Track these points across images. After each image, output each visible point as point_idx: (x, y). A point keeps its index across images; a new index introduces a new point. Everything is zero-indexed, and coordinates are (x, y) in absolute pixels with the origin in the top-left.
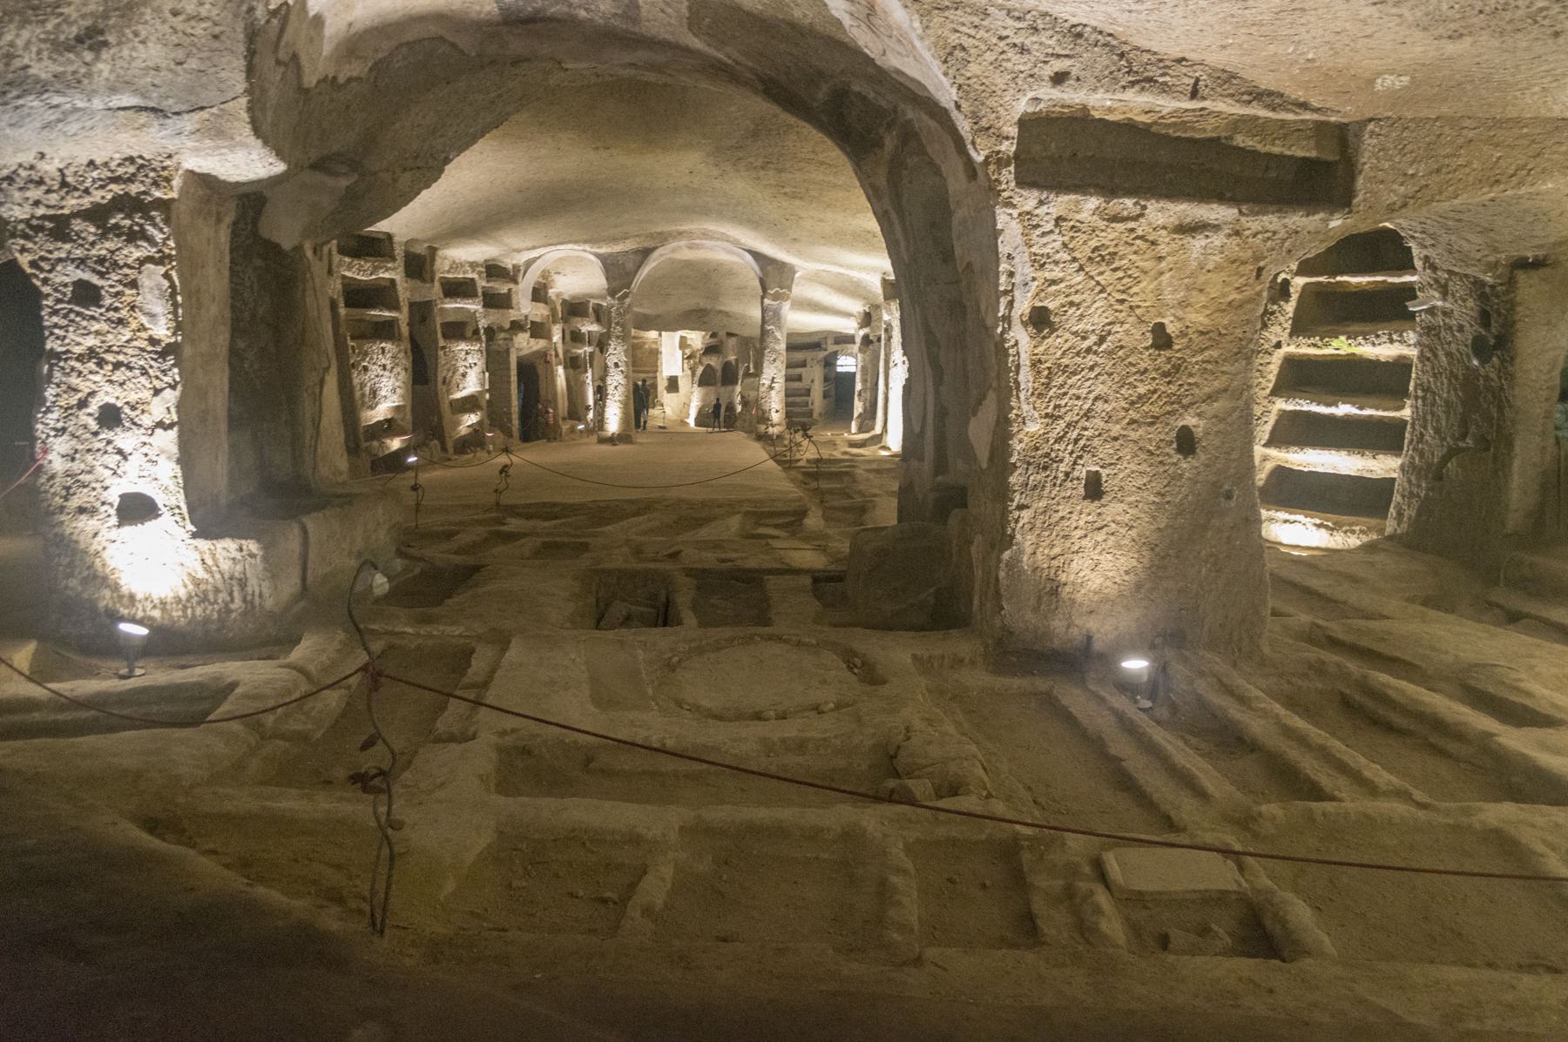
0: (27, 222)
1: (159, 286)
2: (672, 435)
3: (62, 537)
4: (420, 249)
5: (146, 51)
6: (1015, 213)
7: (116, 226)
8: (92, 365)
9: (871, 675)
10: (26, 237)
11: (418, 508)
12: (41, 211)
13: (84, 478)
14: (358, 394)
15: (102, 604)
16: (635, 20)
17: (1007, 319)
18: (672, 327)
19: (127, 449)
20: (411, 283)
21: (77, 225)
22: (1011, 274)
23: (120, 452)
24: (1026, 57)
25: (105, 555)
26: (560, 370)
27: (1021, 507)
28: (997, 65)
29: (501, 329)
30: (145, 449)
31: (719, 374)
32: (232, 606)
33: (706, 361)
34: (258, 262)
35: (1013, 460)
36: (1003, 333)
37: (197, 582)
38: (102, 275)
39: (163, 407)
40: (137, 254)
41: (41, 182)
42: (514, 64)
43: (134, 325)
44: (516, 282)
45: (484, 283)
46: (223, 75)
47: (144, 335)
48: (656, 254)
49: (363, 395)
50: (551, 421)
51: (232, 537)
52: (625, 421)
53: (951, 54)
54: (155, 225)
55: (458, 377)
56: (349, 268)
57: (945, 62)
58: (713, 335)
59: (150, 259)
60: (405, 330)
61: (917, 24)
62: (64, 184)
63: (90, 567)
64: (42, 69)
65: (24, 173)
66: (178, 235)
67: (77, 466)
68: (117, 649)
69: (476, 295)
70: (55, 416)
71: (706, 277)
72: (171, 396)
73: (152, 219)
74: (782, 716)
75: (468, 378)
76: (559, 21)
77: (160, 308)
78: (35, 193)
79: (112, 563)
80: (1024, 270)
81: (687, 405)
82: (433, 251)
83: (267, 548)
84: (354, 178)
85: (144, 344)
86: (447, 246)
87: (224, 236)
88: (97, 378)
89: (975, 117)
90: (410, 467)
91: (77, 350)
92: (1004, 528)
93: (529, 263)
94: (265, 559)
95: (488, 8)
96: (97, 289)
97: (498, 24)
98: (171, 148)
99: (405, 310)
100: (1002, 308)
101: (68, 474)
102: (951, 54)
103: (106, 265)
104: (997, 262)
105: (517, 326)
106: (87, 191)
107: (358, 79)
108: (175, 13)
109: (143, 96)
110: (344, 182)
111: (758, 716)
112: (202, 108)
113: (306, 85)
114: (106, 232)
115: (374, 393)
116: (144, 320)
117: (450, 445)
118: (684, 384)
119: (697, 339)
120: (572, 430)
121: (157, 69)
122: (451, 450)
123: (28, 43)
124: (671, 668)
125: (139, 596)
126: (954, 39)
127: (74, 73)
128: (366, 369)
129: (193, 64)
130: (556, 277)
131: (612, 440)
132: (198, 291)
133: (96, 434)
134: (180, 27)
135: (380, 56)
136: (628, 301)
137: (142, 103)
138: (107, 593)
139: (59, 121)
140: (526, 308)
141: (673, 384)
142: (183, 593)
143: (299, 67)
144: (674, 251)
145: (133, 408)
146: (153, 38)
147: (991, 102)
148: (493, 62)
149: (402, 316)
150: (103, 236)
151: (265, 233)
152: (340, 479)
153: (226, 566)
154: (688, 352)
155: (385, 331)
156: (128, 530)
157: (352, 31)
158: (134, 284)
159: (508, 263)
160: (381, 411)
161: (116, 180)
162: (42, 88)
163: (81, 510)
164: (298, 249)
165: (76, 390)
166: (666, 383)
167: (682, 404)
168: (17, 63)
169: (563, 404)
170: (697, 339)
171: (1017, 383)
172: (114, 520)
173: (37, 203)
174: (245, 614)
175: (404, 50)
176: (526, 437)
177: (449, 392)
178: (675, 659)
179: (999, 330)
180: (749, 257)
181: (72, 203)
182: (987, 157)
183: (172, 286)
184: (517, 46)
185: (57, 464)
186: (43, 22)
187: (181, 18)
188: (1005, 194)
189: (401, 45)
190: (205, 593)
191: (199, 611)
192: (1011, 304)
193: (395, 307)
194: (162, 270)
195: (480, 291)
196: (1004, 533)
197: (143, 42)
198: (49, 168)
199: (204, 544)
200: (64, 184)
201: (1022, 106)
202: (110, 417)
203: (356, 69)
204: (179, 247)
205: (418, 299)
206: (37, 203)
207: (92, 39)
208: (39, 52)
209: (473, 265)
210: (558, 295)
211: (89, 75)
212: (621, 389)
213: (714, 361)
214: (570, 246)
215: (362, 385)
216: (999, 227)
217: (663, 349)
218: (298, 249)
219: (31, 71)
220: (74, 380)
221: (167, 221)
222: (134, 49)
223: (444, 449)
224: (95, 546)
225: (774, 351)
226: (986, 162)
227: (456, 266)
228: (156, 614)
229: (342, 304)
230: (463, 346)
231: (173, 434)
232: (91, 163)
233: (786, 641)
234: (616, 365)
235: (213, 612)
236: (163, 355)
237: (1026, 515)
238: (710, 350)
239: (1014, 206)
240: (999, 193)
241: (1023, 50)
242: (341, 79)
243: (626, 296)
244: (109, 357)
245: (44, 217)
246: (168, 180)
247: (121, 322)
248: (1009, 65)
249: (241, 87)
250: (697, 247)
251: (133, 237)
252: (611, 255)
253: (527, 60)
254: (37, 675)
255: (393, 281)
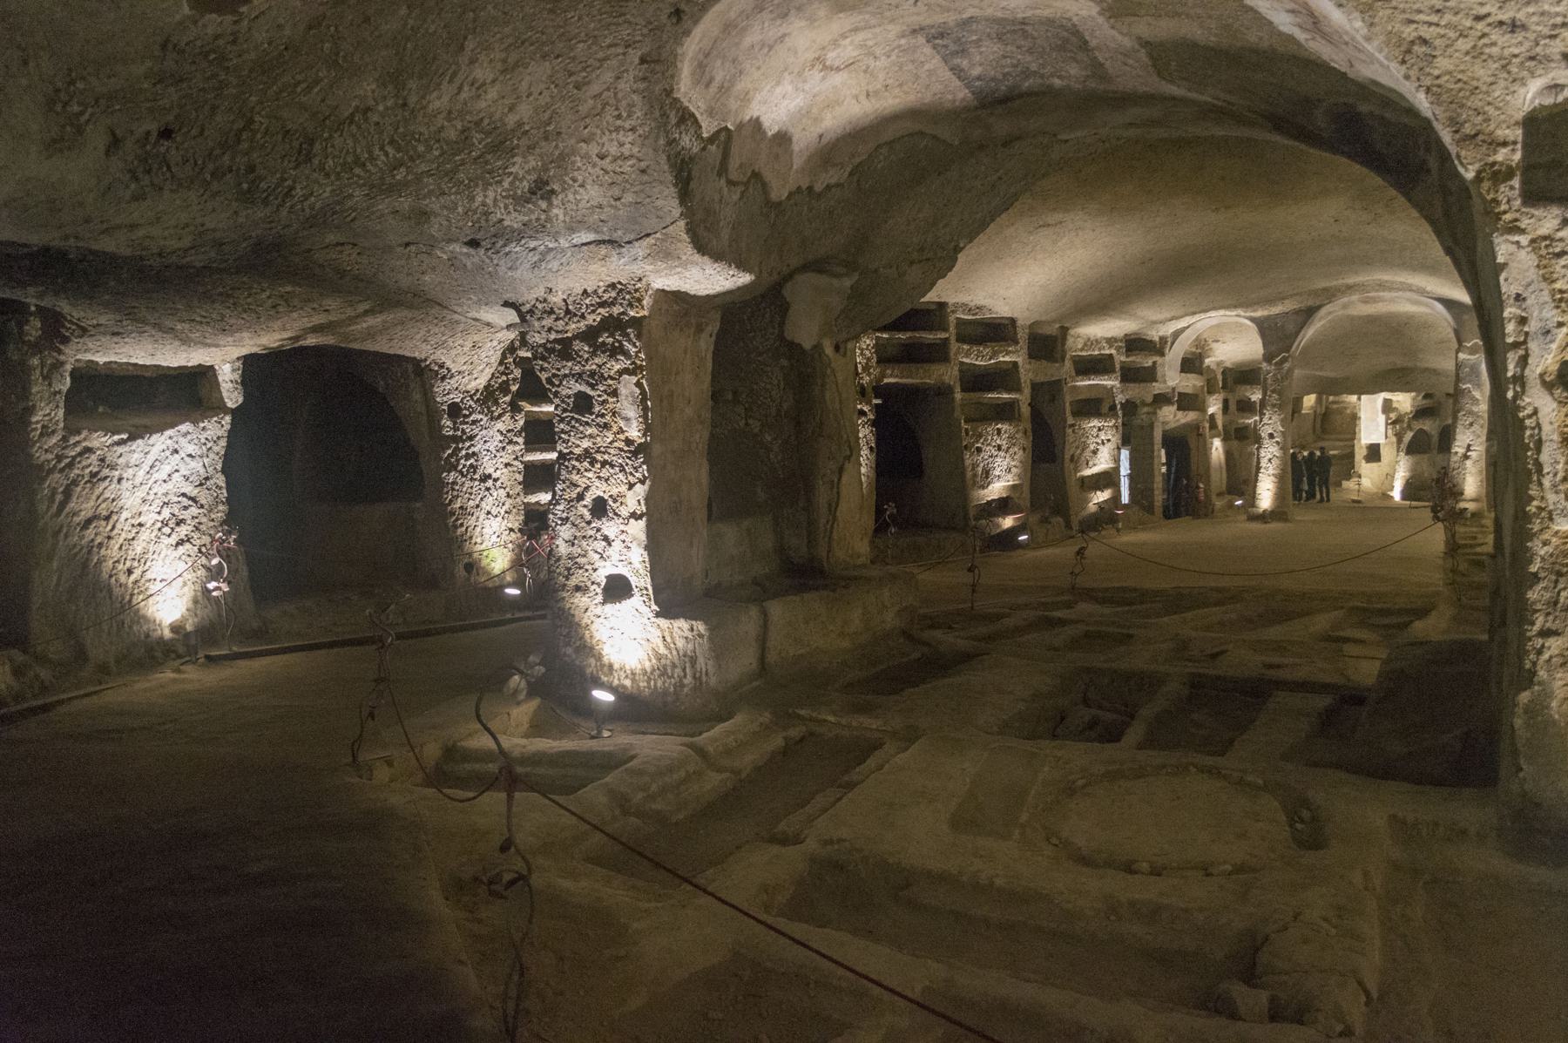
0: (544, 345)
1: (632, 394)
2: (1374, 509)
3: (562, 610)
4: (1052, 330)
5: (587, 193)
6: (1524, 240)
7: (604, 343)
8: (586, 464)
9: (1310, 834)
10: (544, 359)
11: (974, 588)
12: (553, 336)
13: (581, 560)
14: (969, 474)
15: (589, 671)
16: (1104, 77)
17: (1520, 380)
18: (1373, 391)
19: (612, 537)
20: (1036, 364)
21: (577, 345)
22: (1523, 321)
23: (606, 539)
24: (1519, 36)
25: (593, 627)
26: (1217, 443)
27: (1546, 633)
28: (1476, 53)
29: (1144, 404)
30: (623, 537)
31: (1435, 439)
32: (685, 682)
33: (1417, 426)
34: (784, 362)
35: (1533, 568)
36: (1515, 397)
37: (659, 657)
38: (593, 387)
39: (635, 499)
40: (617, 367)
41: (552, 312)
42: (1005, 144)
43: (615, 429)
44: (1162, 354)
45: (1123, 358)
46: (659, 203)
47: (622, 437)
48: (1323, 311)
49: (975, 475)
50: (1202, 497)
51: (686, 618)
52: (1280, 496)
53: (1407, 51)
54: (629, 341)
55: (1087, 453)
56: (967, 356)
57: (1403, 62)
58: (1426, 396)
59: (626, 371)
60: (1025, 410)
61: (1358, 24)
62: (568, 312)
63: (582, 638)
64: (513, 220)
65: (540, 306)
66: (647, 348)
67: (576, 550)
68: (587, 710)
69: (1113, 371)
70: (561, 507)
71: (1396, 331)
72: (641, 490)
73: (628, 335)
74: (1156, 872)
75: (1100, 455)
76: (1036, 94)
77: (632, 412)
78: (548, 322)
79: (597, 636)
80: (1542, 312)
81: (1390, 477)
82: (1064, 331)
83: (711, 629)
84: (856, 276)
85: (621, 445)
86: (1077, 324)
87: (706, 344)
88: (590, 475)
89: (1455, 124)
90: (1021, 546)
91: (577, 451)
92: (1521, 660)
93: (1177, 334)
94: (710, 639)
95: (960, 95)
96: (590, 398)
97: (977, 108)
98: (639, 273)
99: (1027, 391)
100: (1511, 366)
101: (571, 557)
102: (1409, 51)
103: (595, 378)
104: (1501, 306)
105: (1161, 400)
106: (583, 316)
107: (838, 185)
108: (602, 158)
109: (597, 232)
110: (847, 283)
111: (1129, 868)
112: (648, 235)
113: (774, 196)
114: (597, 349)
115: (987, 473)
116: (622, 424)
117: (1076, 526)
118: (1387, 453)
119: (1404, 401)
120: (1231, 506)
121: (600, 207)
122: (1076, 526)
123: (495, 200)
124: (1070, 791)
125: (616, 666)
126: (1409, 32)
127: (538, 219)
128: (979, 450)
129: (629, 198)
130: (1214, 345)
131: (1264, 517)
132: (671, 395)
133: (589, 523)
134: (609, 168)
135: (858, 160)
136: (1287, 365)
137: (598, 237)
138: (592, 661)
139: (541, 261)
140: (1172, 379)
141: (1374, 453)
142: (647, 665)
143: (764, 185)
144: (1345, 307)
145: (615, 501)
146: (589, 181)
147: (1475, 102)
148: (981, 147)
149: (1023, 398)
150: (594, 354)
151: (788, 335)
152: (859, 561)
153: (680, 643)
154: (1393, 416)
155: (1005, 412)
156: (609, 608)
157: (825, 141)
158: (615, 393)
159: (1154, 334)
160: (996, 489)
161: (602, 304)
162: (518, 235)
163: (578, 588)
164: (818, 347)
165: (576, 486)
166: (1364, 452)
167: (1385, 475)
168: (493, 218)
169: (1218, 479)
170: (1404, 401)
171: (1539, 466)
172: (600, 598)
173: (550, 330)
174: (695, 689)
175: (884, 150)
176: (1167, 516)
177: (1077, 470)
178: (1080, 783)
179: (1510, 394)
180: (1439, 307)
181: (574, 327)
182: (1479, 172)
183: (643, 392)
184: (1002, 127)
185: (563, 549)
186: (500, 182)
187: (608, 160)
188: (1508, 217)
189: (879, 146)
190: (665, 667)
191: (659, 683)
192: (1524, 361)
193: (1018, 390)
194: (634, 379)
195: (1118, 366)
196: (1521, 667)
197: (582, 186)
198: (556, 299)
199: (664, 623)
200: (568, 312)
201: (1530, 94)
202: (600, 508)
203: (833, 176)
204: (649, 358)
205: (1041, 378)
206: (550, 330)
207: (541, 189)
208: (506, 207)
209: (1111, 341)
210: (1219, 364)
211: (548, 220)
212: (1276, 462)
213: (1428, 425)
214: (1222, 312)
215: (975, 466)
216: (1500, 260)
217: (1362, 415)
218: (818, 347)
219: (506, 223)
220: (575, 477)
221: (639, 337)
222: (576, 193)
223: (1068, 526)
224: (585, 621)
225: (1471, 413)
226: (1478, 178)
227: (1091, 343)
228: (628, 683)
229: (958, 389)
230: (1095, 423)
231: (642, 523)
232: (585, 291)
233: (1225, 777)
234: (1271, 436)
235: (670, 684)
236: (635, 454)
237: (1554, 645)
238: (1420, 413)
239: (1522, 231)
240: (1498, 216)
241: (1514, 26)
242: (818, 188)
243: (1284, 360)
244: (599, 457)
245: (556, 341)
246: (639, 300)
247: (606, 426)
248: (1495, 50)
249: (677, 212)
250: (1375, 300)
251: (616, 351)
252: (1268, 318)
253: (1019, 138)
254: (537, 728)
255: (1015, 364)
